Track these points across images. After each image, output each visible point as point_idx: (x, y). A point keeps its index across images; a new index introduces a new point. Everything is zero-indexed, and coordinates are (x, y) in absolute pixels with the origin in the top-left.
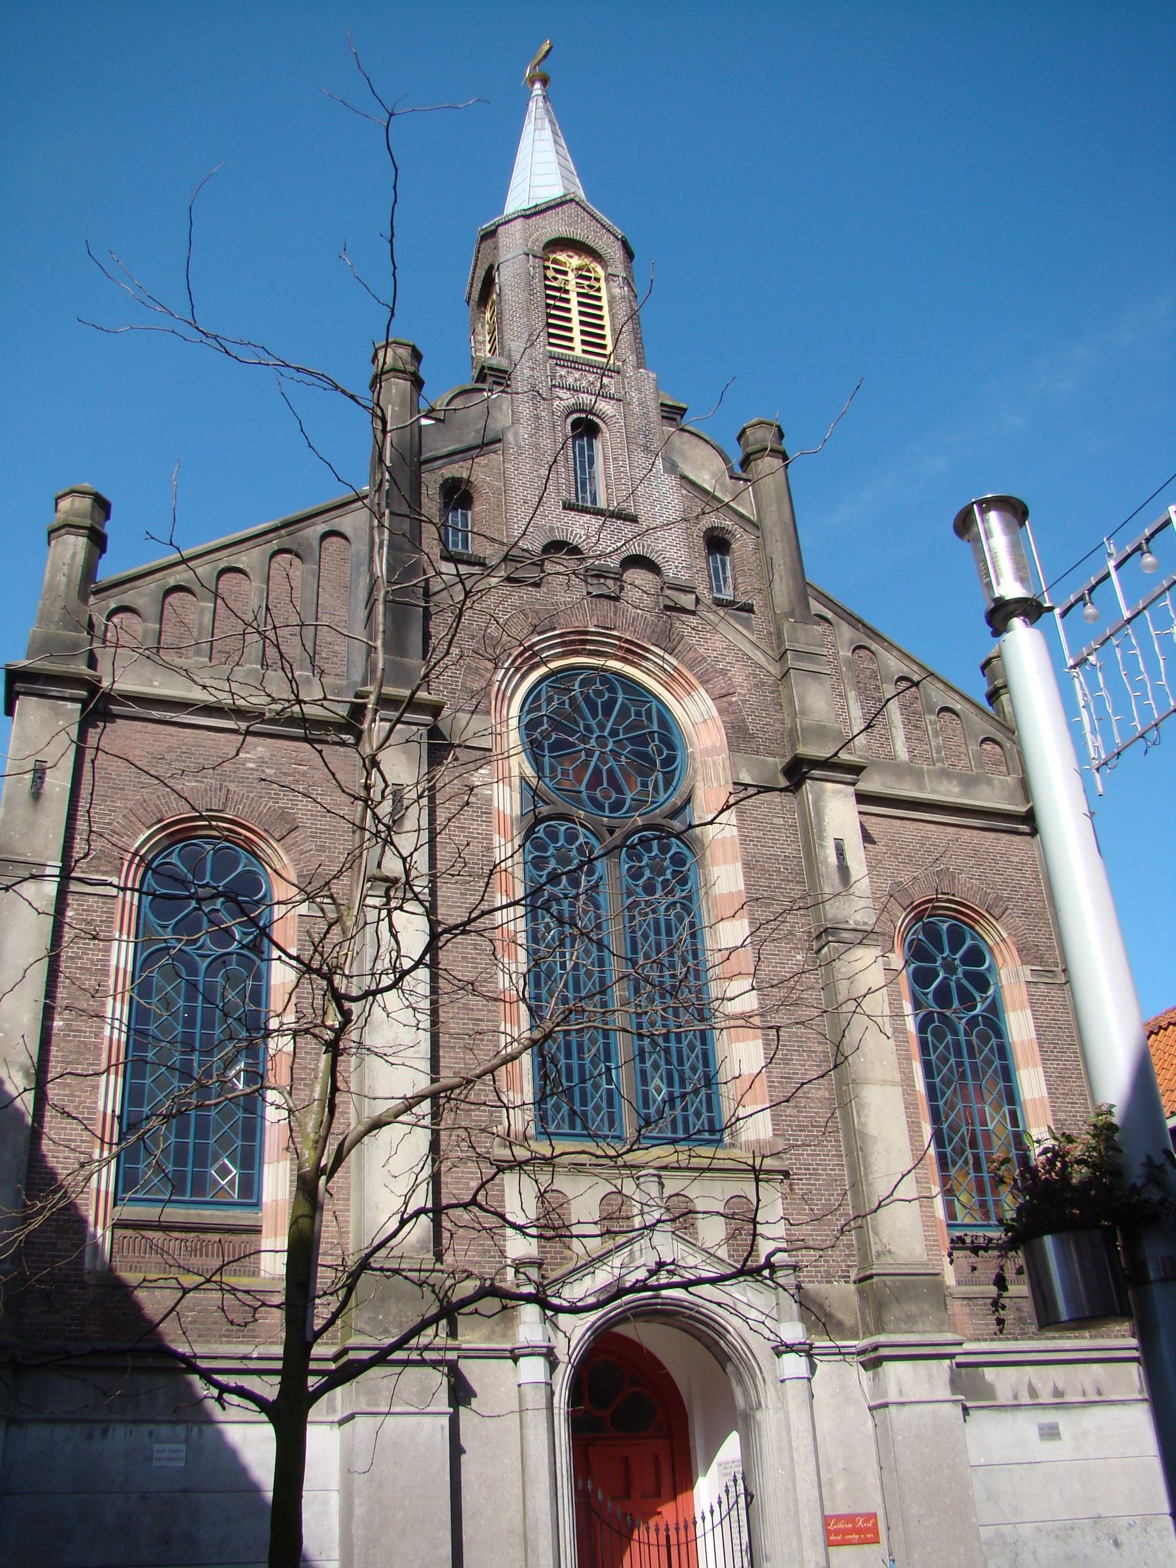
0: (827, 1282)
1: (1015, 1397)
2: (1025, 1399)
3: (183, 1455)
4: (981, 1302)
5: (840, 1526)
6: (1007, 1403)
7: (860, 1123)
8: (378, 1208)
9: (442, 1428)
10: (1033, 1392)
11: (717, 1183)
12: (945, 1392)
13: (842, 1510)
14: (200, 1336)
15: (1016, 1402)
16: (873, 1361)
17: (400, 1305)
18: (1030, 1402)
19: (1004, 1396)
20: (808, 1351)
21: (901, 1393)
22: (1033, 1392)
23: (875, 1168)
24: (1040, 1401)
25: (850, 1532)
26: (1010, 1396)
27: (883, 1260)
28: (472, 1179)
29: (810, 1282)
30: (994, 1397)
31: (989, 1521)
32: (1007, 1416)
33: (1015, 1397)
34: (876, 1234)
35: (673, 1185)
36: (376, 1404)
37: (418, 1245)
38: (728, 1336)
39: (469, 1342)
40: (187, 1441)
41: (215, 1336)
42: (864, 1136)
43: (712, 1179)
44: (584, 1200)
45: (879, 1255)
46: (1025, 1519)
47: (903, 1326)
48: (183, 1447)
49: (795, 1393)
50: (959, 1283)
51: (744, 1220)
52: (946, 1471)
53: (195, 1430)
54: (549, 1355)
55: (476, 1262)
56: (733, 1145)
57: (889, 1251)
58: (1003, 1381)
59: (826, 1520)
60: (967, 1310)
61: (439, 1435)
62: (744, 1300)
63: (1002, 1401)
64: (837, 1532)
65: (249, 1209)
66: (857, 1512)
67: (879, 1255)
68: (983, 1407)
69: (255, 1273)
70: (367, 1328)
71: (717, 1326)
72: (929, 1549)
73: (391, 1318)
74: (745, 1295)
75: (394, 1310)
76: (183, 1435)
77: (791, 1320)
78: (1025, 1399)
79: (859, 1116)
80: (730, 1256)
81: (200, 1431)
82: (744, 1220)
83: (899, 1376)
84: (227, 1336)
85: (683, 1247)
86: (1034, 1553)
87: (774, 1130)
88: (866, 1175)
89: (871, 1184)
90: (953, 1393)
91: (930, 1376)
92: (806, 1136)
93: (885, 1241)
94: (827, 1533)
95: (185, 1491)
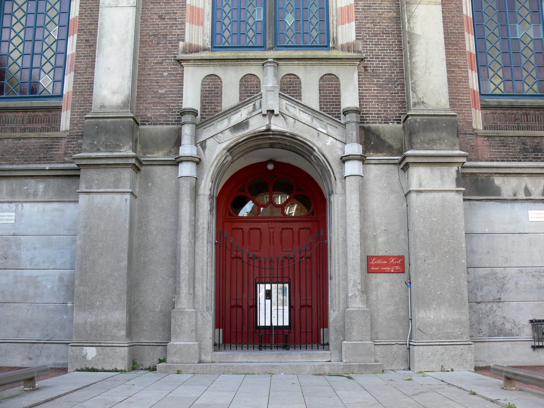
0: (385, 123)
1: (515, 195)
2: (521, 196)
3: (14, 218)
4: (497, 139)
5: (379, 262)
6: (508, 198)
7: (409, 27)
8: (101, 87)
9: (126, 200)
10: (527, 192)
11: (316, 67)
12: (453, 187)
13: (381, 253)
14: (25, 161)
15: (515, 198)
16: (405, 167)
17: (107, 136)
18: (525, 198)
19: (506, 193)
20: (362, 159)
21: (420, 185)
22: (527, 192)
23: (417, 53)
24: (532, 197)
25: (385, 266)
26: (511, 193)
27: (418, 107)
28: (165, 71)
29: (373, 123)
30: (499, 195)
31: (488, 265)
32: (508, 206)
33: (515, 195)
34: (414, 92)
35: (286, 69)
36: (91, 188)
37: (122, 105)
38: (314, 153)
39: (156, 157)
40: (15, 211)
41: (32, 161)
42: (411, 35)
43: (312, 65)
44: (231, 80)
45: (415, 104)
46: (512, 264)
47: (426, 146)
48: (14, 214)
49: (352, 185)
50: (485, 128)
51: (330, 89)
52: (447, 232)
53: (20, 206)
54: (198, 162)
55: (164, 116)
56: (334, 48)
57: (423, 102)
58: (507, 186)
59: (369, 258)
60: (487, 143)
61: (124, 204)
62: (325, 132)
63: (505, 196)
64: (376, 265)
65: (58, 99)
66: (391, 255)
67: (415, 104)
68: (491, 200)
69: (58, 130)
70: (88, 149)
71: (308, 147)
72: (429, 276)
73: (101, 143)
74: (326, 128)
75: (103, 139)
76: (14, 208)
77: (352, 142)
78: (521, 196)
79: (409, 23)
80: (321, 108)
81: (22, 206)
82: (330, 89)
83: (419, 176)
84: (39, 161)
85: (287, 102)
86: (516, 284)
87: (357, 36)
88: (411, 58)
89: (414, 63)
90: (458, 186)
91: (442, 176)
92: (378, 39)
93: (420, 96)
94: (369, 266)
95: (14, 235)
